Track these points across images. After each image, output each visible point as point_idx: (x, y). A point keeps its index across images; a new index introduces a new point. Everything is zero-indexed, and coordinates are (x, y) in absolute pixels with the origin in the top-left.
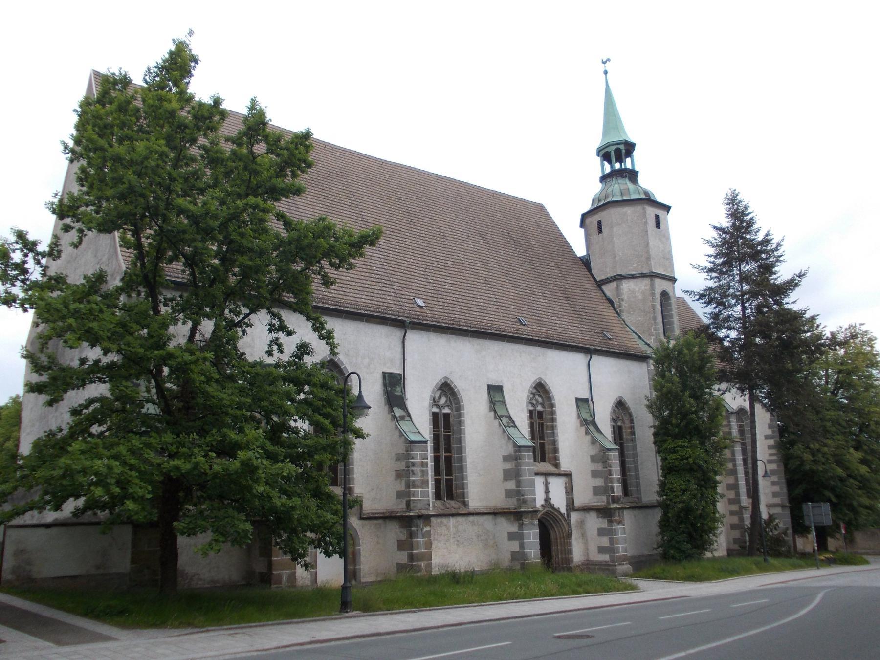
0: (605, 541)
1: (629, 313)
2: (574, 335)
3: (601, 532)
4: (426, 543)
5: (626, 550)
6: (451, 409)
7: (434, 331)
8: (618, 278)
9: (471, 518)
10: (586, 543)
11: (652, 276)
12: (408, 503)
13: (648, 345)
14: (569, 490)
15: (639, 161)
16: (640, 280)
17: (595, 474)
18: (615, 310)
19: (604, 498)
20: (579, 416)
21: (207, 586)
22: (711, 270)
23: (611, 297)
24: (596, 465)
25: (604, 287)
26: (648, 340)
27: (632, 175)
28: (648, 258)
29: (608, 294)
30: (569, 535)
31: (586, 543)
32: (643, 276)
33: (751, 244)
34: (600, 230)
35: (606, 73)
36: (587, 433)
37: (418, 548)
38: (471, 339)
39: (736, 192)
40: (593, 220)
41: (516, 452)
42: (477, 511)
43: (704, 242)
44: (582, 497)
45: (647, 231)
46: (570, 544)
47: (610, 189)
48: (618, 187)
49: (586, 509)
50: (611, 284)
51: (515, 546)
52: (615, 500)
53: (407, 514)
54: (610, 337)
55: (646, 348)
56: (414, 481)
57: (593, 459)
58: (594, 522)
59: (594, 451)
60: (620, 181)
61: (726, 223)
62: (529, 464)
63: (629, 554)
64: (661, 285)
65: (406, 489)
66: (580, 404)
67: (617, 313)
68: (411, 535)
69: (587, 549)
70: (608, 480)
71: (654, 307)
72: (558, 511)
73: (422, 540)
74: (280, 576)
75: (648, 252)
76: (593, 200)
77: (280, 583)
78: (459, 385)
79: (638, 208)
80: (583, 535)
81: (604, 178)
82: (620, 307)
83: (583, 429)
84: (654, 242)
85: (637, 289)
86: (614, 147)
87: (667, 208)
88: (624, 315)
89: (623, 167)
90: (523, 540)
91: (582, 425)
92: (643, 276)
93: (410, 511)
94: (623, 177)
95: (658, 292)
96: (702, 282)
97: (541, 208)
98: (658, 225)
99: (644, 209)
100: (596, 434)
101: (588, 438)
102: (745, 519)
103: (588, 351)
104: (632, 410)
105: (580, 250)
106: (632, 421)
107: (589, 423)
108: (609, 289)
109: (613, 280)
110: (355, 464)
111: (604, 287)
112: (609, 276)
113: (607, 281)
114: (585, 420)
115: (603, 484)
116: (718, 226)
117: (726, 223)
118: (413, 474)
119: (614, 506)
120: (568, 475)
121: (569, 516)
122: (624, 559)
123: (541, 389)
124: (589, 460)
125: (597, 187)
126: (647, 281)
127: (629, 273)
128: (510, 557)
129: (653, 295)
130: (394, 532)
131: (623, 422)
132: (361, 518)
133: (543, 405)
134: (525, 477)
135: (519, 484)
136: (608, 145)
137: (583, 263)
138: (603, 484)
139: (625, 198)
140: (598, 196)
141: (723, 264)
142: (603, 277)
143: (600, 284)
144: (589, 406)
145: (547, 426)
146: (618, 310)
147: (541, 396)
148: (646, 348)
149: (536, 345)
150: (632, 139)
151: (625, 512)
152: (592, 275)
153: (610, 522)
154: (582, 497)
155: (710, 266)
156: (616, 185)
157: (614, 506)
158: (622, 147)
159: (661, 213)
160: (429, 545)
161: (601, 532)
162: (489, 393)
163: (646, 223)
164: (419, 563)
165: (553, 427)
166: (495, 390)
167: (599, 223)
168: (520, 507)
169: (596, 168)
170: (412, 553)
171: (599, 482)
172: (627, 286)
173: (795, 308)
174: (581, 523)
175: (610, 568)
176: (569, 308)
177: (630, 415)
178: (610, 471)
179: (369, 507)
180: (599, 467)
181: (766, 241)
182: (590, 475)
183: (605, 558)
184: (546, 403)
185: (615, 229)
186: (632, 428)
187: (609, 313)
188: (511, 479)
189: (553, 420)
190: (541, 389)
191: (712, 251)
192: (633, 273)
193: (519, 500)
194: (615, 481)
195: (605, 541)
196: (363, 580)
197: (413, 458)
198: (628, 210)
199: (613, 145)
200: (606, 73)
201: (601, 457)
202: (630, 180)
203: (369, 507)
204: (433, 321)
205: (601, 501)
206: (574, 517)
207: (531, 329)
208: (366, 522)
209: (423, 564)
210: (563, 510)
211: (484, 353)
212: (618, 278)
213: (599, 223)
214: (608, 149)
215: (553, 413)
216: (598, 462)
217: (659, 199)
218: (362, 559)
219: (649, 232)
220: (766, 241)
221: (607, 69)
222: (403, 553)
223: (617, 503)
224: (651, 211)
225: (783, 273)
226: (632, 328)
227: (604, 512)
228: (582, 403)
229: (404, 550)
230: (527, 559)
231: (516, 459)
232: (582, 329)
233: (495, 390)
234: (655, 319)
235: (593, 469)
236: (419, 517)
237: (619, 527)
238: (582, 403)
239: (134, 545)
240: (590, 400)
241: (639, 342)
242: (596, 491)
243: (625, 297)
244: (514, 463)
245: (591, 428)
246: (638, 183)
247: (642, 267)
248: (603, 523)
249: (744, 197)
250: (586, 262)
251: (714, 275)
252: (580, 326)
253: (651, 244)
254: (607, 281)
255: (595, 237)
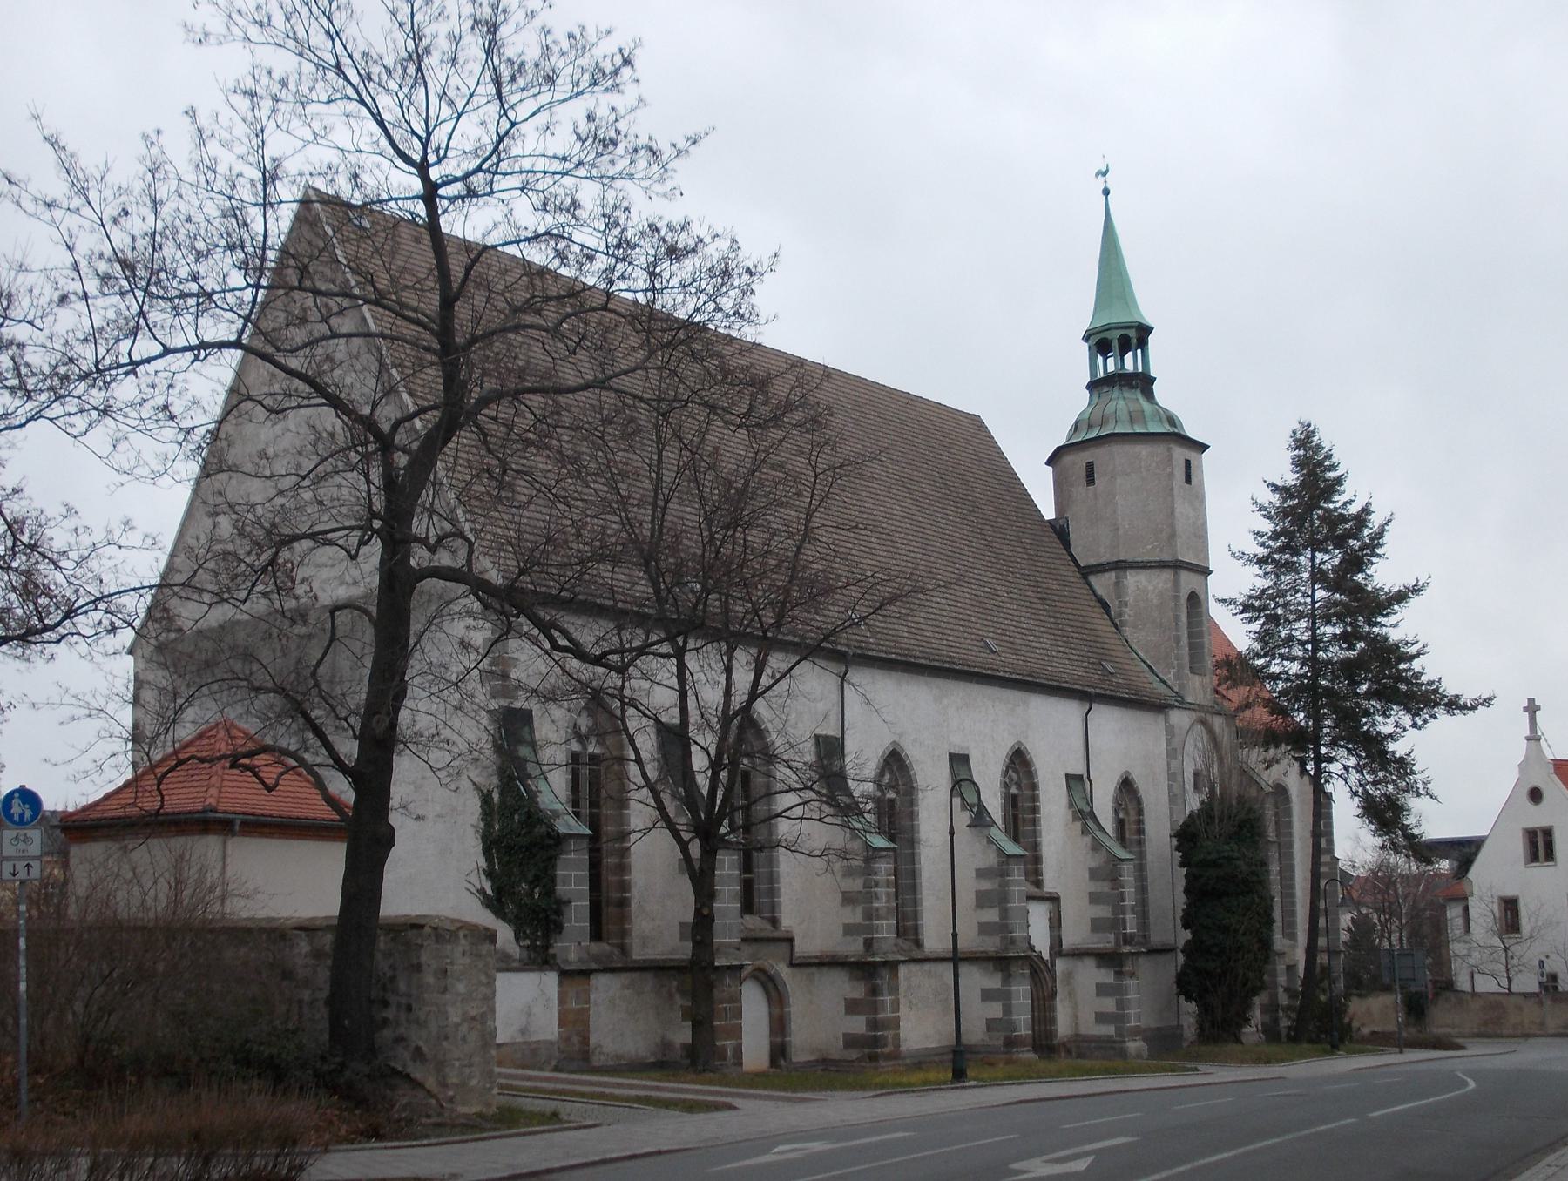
0: (1109, 1005)
1: (1135, 627)
2: (1065, 668)
3: (1102, 990)
4: (892, 1002)
5: (1139, 1019)
6: (897, 793)
7: (880, 668)
8: (1120, 566)
9: (927, 966)
10: (1075, 1006)
11: (1177, 566)
12: (868, 944)
13: (1165, 683)
14: (1056, 923)
15: (1161, 357)
16: (1157, 571)
17: (1094, 898)
18: (1111, 620)
19: (1112, 937)
20: (1071, 804)
21: (611, 1063)
22: (1261, 561)
23: (1105, 598)
24: (1099, 883)
25: (1093, 579)
26: (1165, 674)
27: (1143, 382)
28: (1173, 536)
29: (1100, 591)
30: (1054, 994)
31: (1075, 1006)
32: (1162, 565)
33: (1334, 520)
34: (1090, 480)
35: (1106, 192)
36: (1085, 831)
37: (884, 1010)
38: (929, 679)
39: (1311, 428)
40: (1079, 460)
41: (1001, 864)
42: (936, 956)
43: (1254, 508)
44: (1075, 934)
45: (1172, 489)
46: (1053, 1009)
47: (1111, 408)
48: (1121, 402)
49: (1078, 954)
50: (1107, 575)
51: (995, 1010)
52: (1128, 940)
53: (870, 959)
54: (1112, 670)
55: (1162, 689)
56: (877, 909)
57: (1094, 874)
58: (1089, 976)
59: (1096, 861)
60: (1127, 394)
61: (1291, 478)
62: (1019, 884)
63: (1143, 1024)
64: (1188, 581)
65: (864, 919)
66: (1072, 783)
67: (1116, 626)
68: (874, 991)
69: (1076, 1017)
70: (1119, 909)
71: (1177, 618)
72: (1040, 956)
73: (888, 998)
74: (724, 1047)
75: (1172, 526)
76: (1077, 423)
77: (725, 1059)
78: (912, 753)
79: (1160, 449)
80: (1071, 994)
81: (1094, 386)
82: (1120, 615)
83: (1078, 825)
84: (1181, 508)
85: (1151, 588)
86: (1118, 333)
87: (1203, 447)
88: (1128, 631)
89: (1140, 370)
90: (1010, 999)
91: (1075, 819)
92: (1162, 565)
93: (873, 955)
94: (1132, 387)
95: (1184, 594)
96: (1250, 580)
97: (976, 423)
98: (1188, 479)
99: (1169, 449)
100: (1099, 834)
101: (1088, 839)
102: (1279, 972)
103: (1087, 697)
104: (1142, 793)
105: (1049, 513)
106: (1140, 812)
107: (1084, 816)
108: (1102, 583)
109: (1111, 570)
110: (782, 880)
111: (1093, 579)
112: (1104, 560)
113: (1100, 568)
114: (1081, 811)
115: (1109, 915)
116: (1280, 483)
117: (1291, 478)
118: (877, 898)
119: (1126, 949)
120: (1054, 899)
121: (1053, 964)
122: (1136, 1032)
123: (1019, 761)
124: (1087, 875)
125: (1080, 401)
126: (1167, 575)
127: (1139, 559)
128: (984, 1027)
129: (1176, 598)
130: (840, 987)
131: (1127, 813)
132: (791, 965)
133: (1019, 786)
134: (1014, 904)
135: (1005, 913)
136: (1109, 328)
137: (1055, 531)
138: (1109, 915)
139: (1138, 430)
140: (1087, 416)
141: (1281, 550)
142: (1093, 561)
143: (1086, 572)
144: (1084, 788)
145: (1024, 820)
146: (1117, 621)
147: (1016, 771)
148: (1162, 689)
149: (1013, 688)
150: (1149, 320)
151: (1141, 960)
152: (1071, 555)
153: (1119, 974)
154: (1075, 934)
155: (1262, 552)
156: (1121, 402)
157: (1126, 949)
158: (1132, 333)
159: (1192, 455)
160: (896, 1006)
161: (1102, 990)
162: (951, 767)
163: (1171, 475)
164: (885, 1033)
165: (1035, 822)
166: (959, 761)
167: (1090, 467)
168: (1006, 950)
169: (1077, 364)
170: (875, 1019)
171: (1104, 912)
172: (1133, 580)
173: (1394, 636)
174: (1069, 976)
175: (1117, 1045)
176: (1047, 619)
177: (1139, 801)
178: (1122, 893)
179: (803, 947)
180: (1104, 887)
181: (1362, 518)
182: (1087, 899)
183: (1109, 1030)
184: (1024, 782)
185: (1119, 481)
186: (1140, 822)
187: (1104, 625)
188: (991, 907)
189: (1035, 810)
190: (1019, 761)
191: (1267, 527)
192: (1146, 558)
193: (1003, 939)
194: (1129, 910)
195: (1109, 1005)
196: (794, 1059)
197: (876, 874)
198: (1143, 450)
199: (1116, 328)
200: (1106, 192)
201: (1108, 872)
202: (1143, 392)
203: (803, 947)
204: (879, 651)
205: (1106, 941)
206: (1060, 966)
207: (1006, 661)
208: (795, 970)
209: (889, 1034)
210: (1046, 956)
211: (945, 701)
212: (1120, 566)
213: (1090, 467)
214: (1107, 335)
215: (1035, 798)
216: (1104, 880)
217: (1192, 432)
218: (793, 1027)
219: (1176, 492)
220: (1362, 518)
221: (1109, 186)
222: (855, 1018)
223: (1130, 944)
224: (1180, 454)
225: (1383, 575)
226: (1141, 654)
227: (1106, 958)
228: (1074, 781)
229: (859, 1013)
230: (1015, 1030)
231: (1002, 876)
232: (1072, 657)
233: (959, 761)
234: (1178, 640)
235: (1093, 890)
236: (885, 963)
237: (1131, 982)
238: (1074, 781)
239: (562, 1000)
240: (1085, 776)
241: (1152, 678)
242: (1097, 925)
243: (1130, 599)
244: (997, 880)
245: (1091, 823)
246: (1153, 397)
247: (1161, 551)
248: (1107, 976)
249: (1326, 437)
250: (1060, 530)
251: (1270, 568)
252: (1067, 651)
253: (1177, 510)
254: (1100, 568)
255: (1080, 490)
